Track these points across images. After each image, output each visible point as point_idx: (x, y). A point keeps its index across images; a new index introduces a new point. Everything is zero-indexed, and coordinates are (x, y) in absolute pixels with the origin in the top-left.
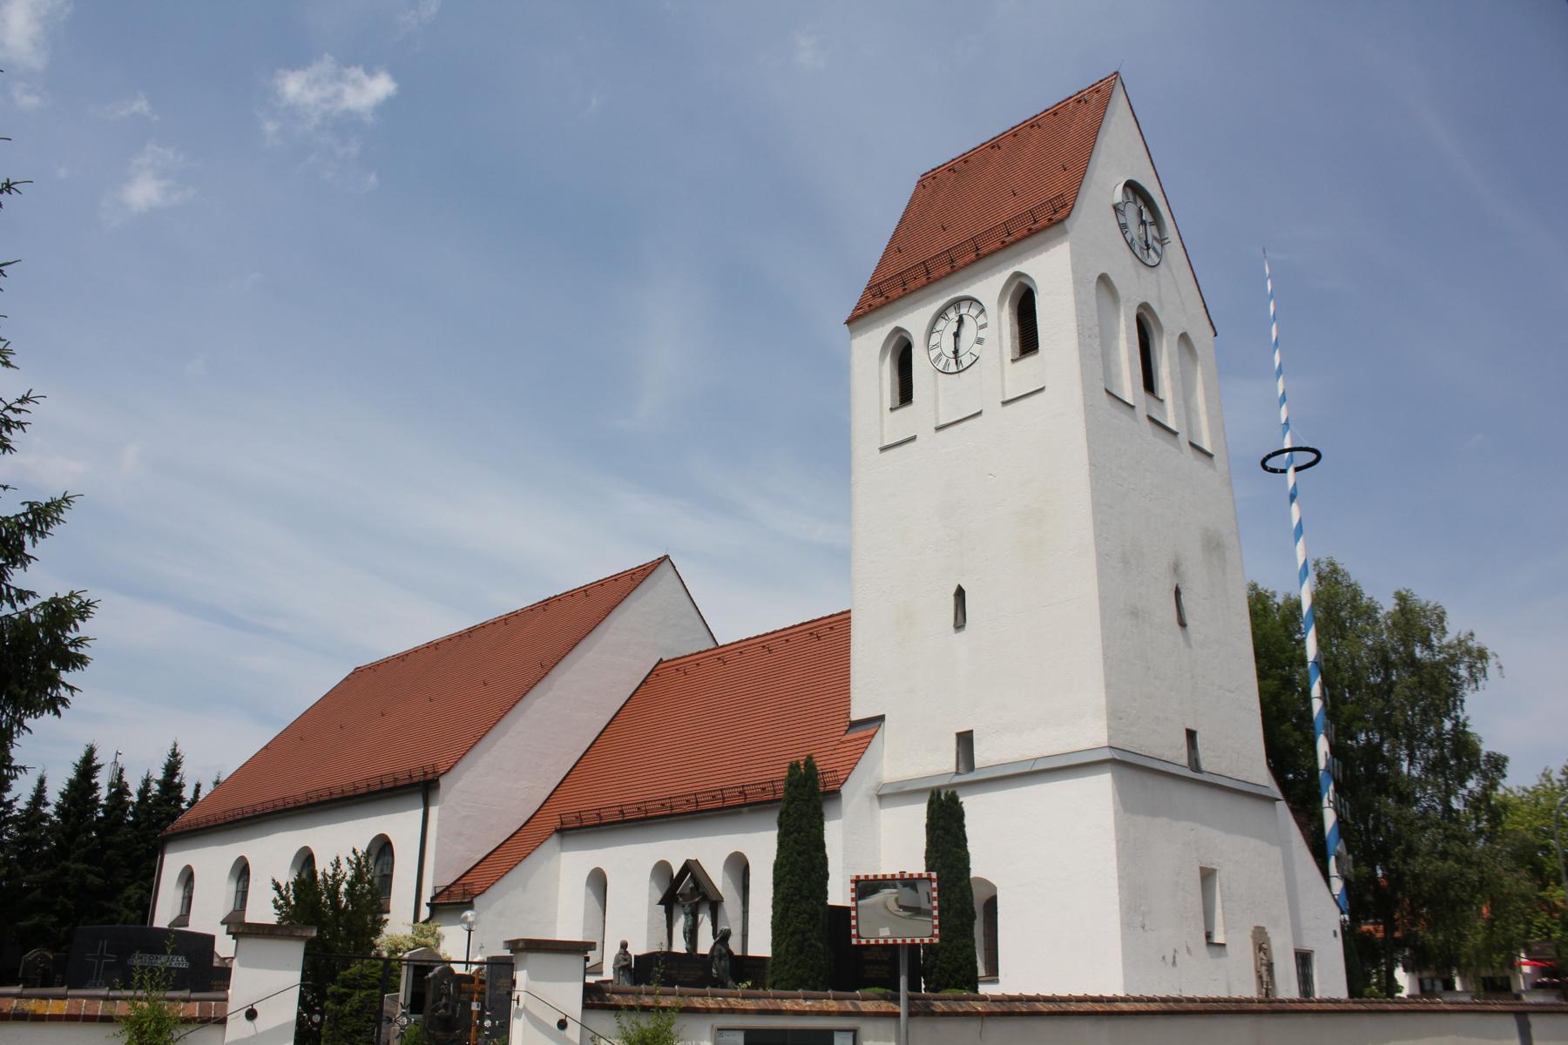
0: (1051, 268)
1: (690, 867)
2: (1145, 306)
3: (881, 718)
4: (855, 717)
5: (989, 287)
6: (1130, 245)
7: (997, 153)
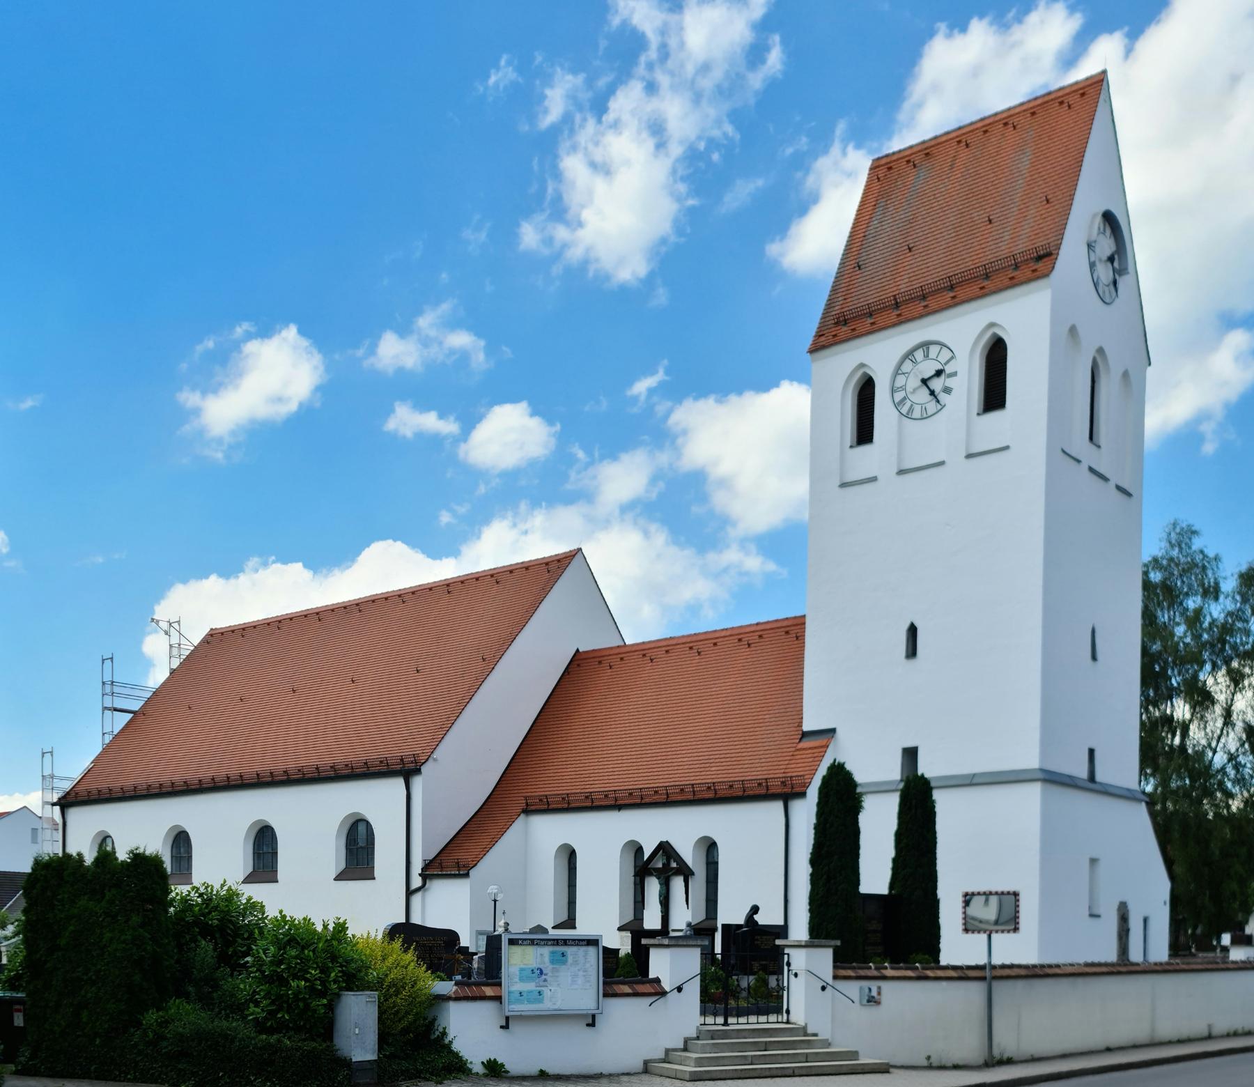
0: (1024, 316)
1: (664, 848)
2: (1101, 351)
3: (833, 731)
4: (807, 726)
5: (960, 332)
6: (1096, 285)
7: (964, 154)
